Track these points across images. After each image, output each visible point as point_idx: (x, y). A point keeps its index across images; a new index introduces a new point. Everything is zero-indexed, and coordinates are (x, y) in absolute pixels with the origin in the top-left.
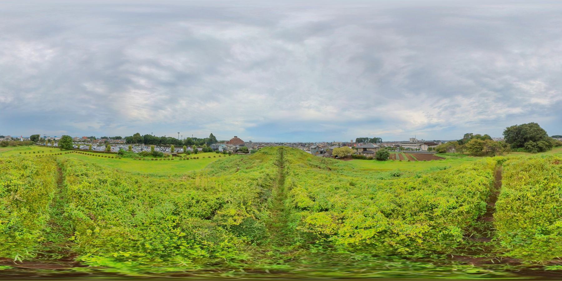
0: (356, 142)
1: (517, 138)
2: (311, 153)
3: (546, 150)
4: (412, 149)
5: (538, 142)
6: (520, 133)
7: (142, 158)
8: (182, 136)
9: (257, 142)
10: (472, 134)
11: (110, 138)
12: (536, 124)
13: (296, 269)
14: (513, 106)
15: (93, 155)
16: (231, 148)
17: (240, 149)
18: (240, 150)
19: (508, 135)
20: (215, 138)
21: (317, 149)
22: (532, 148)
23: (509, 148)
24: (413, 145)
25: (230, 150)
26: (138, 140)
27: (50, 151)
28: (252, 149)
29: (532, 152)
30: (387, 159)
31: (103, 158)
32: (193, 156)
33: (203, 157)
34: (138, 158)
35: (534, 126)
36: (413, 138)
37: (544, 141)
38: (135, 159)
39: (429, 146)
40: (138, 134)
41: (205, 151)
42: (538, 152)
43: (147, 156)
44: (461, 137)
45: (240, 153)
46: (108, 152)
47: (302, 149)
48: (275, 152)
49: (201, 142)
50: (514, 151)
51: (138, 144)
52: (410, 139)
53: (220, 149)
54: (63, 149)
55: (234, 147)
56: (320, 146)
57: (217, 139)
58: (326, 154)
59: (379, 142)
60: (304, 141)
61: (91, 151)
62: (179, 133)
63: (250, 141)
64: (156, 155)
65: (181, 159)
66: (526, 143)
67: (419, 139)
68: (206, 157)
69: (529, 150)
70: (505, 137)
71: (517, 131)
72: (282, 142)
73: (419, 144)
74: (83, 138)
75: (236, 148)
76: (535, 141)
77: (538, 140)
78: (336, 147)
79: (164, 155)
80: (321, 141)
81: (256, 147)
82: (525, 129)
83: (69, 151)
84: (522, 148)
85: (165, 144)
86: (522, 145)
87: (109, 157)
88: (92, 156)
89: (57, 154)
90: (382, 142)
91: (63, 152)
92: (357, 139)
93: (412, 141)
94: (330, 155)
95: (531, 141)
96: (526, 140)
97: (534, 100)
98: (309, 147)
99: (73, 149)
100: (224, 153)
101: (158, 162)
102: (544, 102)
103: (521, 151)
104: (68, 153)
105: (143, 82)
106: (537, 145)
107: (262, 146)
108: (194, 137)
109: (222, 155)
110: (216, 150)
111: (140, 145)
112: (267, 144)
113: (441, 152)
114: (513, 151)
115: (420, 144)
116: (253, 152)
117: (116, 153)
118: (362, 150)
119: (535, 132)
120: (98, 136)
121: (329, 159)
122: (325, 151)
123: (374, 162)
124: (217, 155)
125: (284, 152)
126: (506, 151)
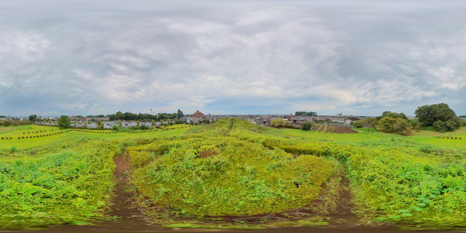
0: (295, 115)
1: (427, 117)
2: (256, 123)
3: (454, 130)
5: (447, 122)
6: (430, 113)
8: (155, 112)
9: (215, 115)
10: (390, 112)
11: (93, 116)
12: (446, 105)
13: (354, 207)
14: (428, 89)
15: (92, 132)
16: (196, 120)
18: (203, 121)
19: (420, 114)
20: (182, 113)
21: (261, 119)
22: (440, 127)
23: (419, 126)
24: (339, 119)
25: (196, 122)
27: (52, 130)
28: (212, 120)
29: (440, 131)
30: (310, 129)
32: (170, 127)
33: (178, 128)
34: (131, 131)
35: (444, 107)
36: (340, 114)
38: (129, 133)
39: (353, 120)
40: (120, 112)
41: (177, 123)
42: (446, 131)
43: (137, 129)
44: (380, 114)
46: (102, 128)
48: (228, 121)
49: (173, 117)
50: (424, 130)
52: (338, 114)
53: (188, 121)
55: (199, 119)
58: (267, 124)
59: (314, 116)
62: (151, 110)
63: (209, 114)
65: (163, 130)
67: (344, 115)
68: (180, 127)
69: (438, 129)
70: (417, 116)
71: (427, 110)
72: (235, 115)
73: (344, 119)
75: (200, 120)
76: (443, 121)
77: (447, 120)
79: (149, 128)
81: (214, 119)
83: (68, 129)
84: (431, 127)
85: (142, 120)
87: (107, 133)
90: (316, 115)
91: (64, 131)
93: (338, 116)
94: (269, 125)
95: (440, 121)
96: (435, 119)
97: (444, 85)
99: (71, 127)
102: (453, 87)
103: (430, 130)
104: (68, 131)
105: (122, 68)
107: (219, 118)
108: (164, 112)
109: (191, 126)
110: (185, 122)
112: (223, 116)
113: (358, 127)
114: (422, 130)
115: (345, 119)
116: (213, 122)
117: (111, 129)
118: (293, 122)
123: (299, 131)
124: (187, 126)
125: (234, 122)
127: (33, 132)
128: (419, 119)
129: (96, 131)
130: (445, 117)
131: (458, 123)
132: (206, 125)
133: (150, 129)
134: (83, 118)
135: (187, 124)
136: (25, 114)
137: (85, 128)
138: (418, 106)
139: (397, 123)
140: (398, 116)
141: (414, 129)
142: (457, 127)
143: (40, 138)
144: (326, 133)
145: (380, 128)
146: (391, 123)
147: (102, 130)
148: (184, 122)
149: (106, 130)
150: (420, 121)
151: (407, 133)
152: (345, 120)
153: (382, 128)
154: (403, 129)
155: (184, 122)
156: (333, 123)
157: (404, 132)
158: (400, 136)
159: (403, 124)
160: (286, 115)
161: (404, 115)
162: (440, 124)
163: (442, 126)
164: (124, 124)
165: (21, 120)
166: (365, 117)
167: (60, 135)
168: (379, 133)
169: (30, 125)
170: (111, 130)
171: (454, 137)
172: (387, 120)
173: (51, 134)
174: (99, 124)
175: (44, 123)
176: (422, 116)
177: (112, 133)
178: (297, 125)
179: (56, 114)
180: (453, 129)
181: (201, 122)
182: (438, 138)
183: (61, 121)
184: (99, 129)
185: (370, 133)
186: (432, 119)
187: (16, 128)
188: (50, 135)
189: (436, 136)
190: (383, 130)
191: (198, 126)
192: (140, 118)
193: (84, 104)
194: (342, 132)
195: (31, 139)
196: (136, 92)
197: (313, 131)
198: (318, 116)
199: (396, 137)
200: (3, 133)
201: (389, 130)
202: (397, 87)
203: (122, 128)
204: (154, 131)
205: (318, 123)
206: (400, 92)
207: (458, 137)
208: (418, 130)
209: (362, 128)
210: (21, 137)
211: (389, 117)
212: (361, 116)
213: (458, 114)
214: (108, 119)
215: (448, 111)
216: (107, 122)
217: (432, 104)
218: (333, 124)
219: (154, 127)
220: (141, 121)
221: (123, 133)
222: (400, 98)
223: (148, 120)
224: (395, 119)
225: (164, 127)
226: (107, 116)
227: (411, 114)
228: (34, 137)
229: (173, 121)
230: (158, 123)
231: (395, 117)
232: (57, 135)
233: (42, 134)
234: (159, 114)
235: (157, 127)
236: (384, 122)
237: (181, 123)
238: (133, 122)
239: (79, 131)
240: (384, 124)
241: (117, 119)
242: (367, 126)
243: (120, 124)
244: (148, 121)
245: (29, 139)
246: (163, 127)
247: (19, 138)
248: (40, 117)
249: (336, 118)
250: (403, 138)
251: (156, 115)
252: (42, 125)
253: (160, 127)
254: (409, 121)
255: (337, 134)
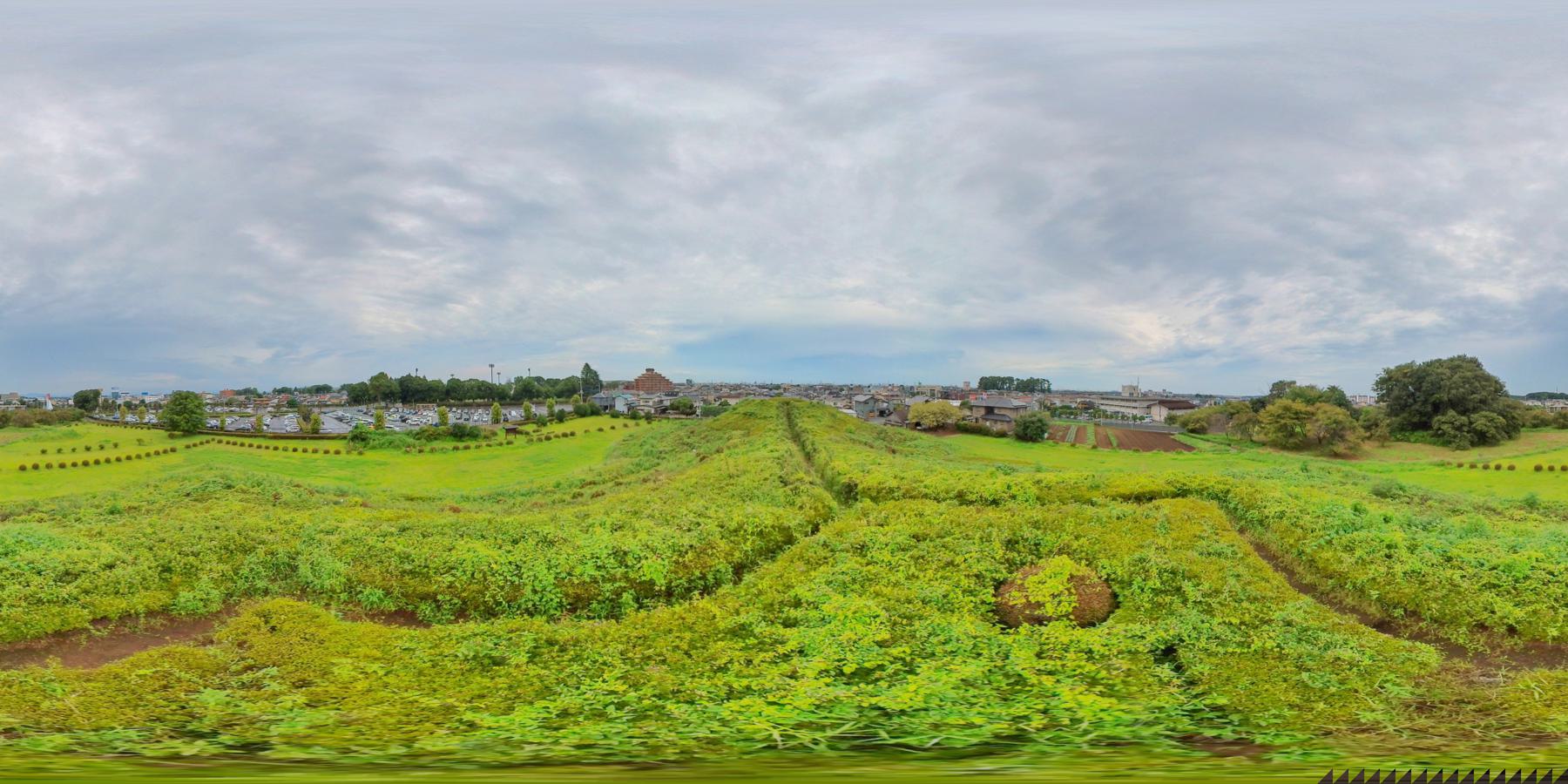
1: (1411, 401)
2: (855, 416)
3: (1498, 441)
4: (1123, 417)
5: (1474, 416)
7: (425, 445)
8: (505, 373)
10: (1294, 383)
11: (296, 389)
12: (1474, 361)
14: (1418, 300)
15: (276, 449)
16: (648, 402)
17: (672, 405)
18: (674, 407)
19: (1390, 391)
20: (597, 376)
22: (1452, 432)
23: (1386, 431)
26: (384, 393)
30: (1042, 438)
31: (309, 455)
32: (557, 428)
33: (586, 431)
34: (414, 447)
35: (1466, 367)
37: (1493, 411)
38: (407, 452)
39: (1173, 409)
40: (382, 375)
41: (581, 413)
42: (1473, 444)
43: (436, 439)
44: (1263, 391)
45: (672, 414)
46: (316, 434)
47: (832, 404)
49: (566, 390)
50: (1402, 440)
51: (383, 404)
52: (1124, 387)
53: (620, 406)
54: (176, 433)
55: (657, 399)
56: (880, 397)
57: (601, 378)
58: (893, 418)
59: (1043, 391)
60: (837, 380)
61: (264, 437)
62: (492, 366)
63: (689, 381)
64: (460, 434)
65: (532, 440)
66: (1436, 419)
67: (1143, 388)
69: (1446, 438)
70: (1381, 399)
72: (776, 382)
74: (223, 393)
75: (661, 401)
76: (1464, 412)
77: (1475, 410)
78: (920, 399)
79: (483, 434)
80: (885, 382)
82: (1437, 374)
83: (197, 439)
84: (1425, 433)
85: (461, 400)
86: (1426, 423)
87: (326, 452)
88: (271, 451)
89: (161, 451)
90: (1049, 391)
91: (180, 443)
92: (982, 379)
93: (1126, 395)
94: (903, 421)
95: (1452, 413)
96: (1438, 408)
97: (1470, 289)
98: (850, 397)
100: (634, 417)
101: (472, 453)
102: (1503, 292)
103: (1421, 442)
104: (195, 445)
106: (1471, 423)
109: (631, 423)
110: (608, 409)
111: (390, 405)
113: (1193, 431)
114: (1398, 440)
117: (345, 438)
118: (983, 412)
119: (1467, 386)
120: (265, 387)
121: (900, 430)
122: (892, 410)
123: (1007, 443)
124: (619, 422)
126: (1375, 440)
127: (74, 450)
128: (1388, 406)
129: (292, 444)
130: (1470, 400)
131: (1513, 418)
132: (687, 422)
133: (486, 437)
134: (260, 396)
135: (615, 415)
136: (61, 386)
137: (256, 432)
138: (1385, 367)
139: (1317, 420)
140: (1320, 397)
141: (1369, 438)
142: (1507, 433)
143: (93, 469)
144: (1093, 452)
145: (1266, 435)
146: (1297, 419)
147: (312, 442)
148: (606, 408)
149: (325, 442)
150: (1392, 412)
151: (1345, 451)
152: (1149, 407)
153: (1272, 436)
154: (1337, 438)
155: (606, 408)
156: (1107, 417)
157: (1340, 448)
158: (1325, 459)
159: (1335, 422)
160: (948, 388)
161: (1342, 395)
162: (1453, 423)
163: (1459, 429)
164: (396, 416)
165: (50, 407)
166: (1211, 396)
167: (163, 458)
168: (1260, 450)
169: (73, 424)
170: (345, 442)
171: (1492, 465)
172: (1287, 409)
173: (134, 456)
174: (306, 418)
175: (123, 415)
176: (1398, 398)
177: (348, 452)
178: (999, 423)
179: (159, 385)
180: (1493, 437)
181: (664, 411)
182: (1443, 465)
183: (172, 410)
184: (304, 438)
185: (1234, 451)
186: (1429, 408)
187: (25, 432)
188: (129, 458)
189: (1436, 459)
190: (1273, 441)
191: (655, 424)
192: (453, 394)
193: (264, 344)
194: (1148, 448)
195: (62, 470)
196: (450, 306)
197: (1051, 442)
198: (1057, 392)
199: (1317, 463)
200: (1544, 452)
201: (1291, 440)
202: (1312, 295)
203: (384, 435)
204: (501, 444)
205: (1060, 416)
206: (1323, 313)
207: (1505, 464)
208: (1383, 440)
209: (1204, 433)
210: (29, 466)
211: (1294, 400)
212: (1197, 396)
213: (1516, 387)
214: (345, 397)
215: (1480, 382)
216: (338, 409)
217: (1428, 359)
218: (1108, 421)
219: (499, 428)
220: (454, 405)
221: (385, 452)
222: (1328, 336)
223: (479, 401)
224: (1309, 409)
225: (534, 427)
226: (344, 387)
227: (1362, 388)
228: (74, 465)
229: (567, 403)
230: (515, 414)
231: (1310, 401)
232: (155, 459)
233: (102, 456)
234: (519, 380)
235: (509, 431)
236: (1278, 416)
237: (595, 412)
238: (425, 408)
239: (235, 444)
240: (1277, 422)
241: (375, 400)
242: (1223, 430)
243: (379, 419)
244: (479, 406)
245: (56, 471)
246: (530, 428)
247: (23, 468)
248: (116, 396)
249: (1117, 400)
250: (1335, 466)
251: (509, 384)
252: (116, 423)
253: (520, 428)
254: (1355, 414)
255: (1131, 452)
